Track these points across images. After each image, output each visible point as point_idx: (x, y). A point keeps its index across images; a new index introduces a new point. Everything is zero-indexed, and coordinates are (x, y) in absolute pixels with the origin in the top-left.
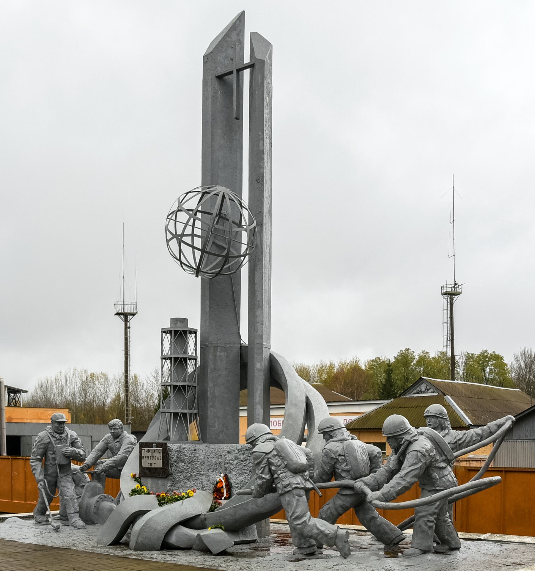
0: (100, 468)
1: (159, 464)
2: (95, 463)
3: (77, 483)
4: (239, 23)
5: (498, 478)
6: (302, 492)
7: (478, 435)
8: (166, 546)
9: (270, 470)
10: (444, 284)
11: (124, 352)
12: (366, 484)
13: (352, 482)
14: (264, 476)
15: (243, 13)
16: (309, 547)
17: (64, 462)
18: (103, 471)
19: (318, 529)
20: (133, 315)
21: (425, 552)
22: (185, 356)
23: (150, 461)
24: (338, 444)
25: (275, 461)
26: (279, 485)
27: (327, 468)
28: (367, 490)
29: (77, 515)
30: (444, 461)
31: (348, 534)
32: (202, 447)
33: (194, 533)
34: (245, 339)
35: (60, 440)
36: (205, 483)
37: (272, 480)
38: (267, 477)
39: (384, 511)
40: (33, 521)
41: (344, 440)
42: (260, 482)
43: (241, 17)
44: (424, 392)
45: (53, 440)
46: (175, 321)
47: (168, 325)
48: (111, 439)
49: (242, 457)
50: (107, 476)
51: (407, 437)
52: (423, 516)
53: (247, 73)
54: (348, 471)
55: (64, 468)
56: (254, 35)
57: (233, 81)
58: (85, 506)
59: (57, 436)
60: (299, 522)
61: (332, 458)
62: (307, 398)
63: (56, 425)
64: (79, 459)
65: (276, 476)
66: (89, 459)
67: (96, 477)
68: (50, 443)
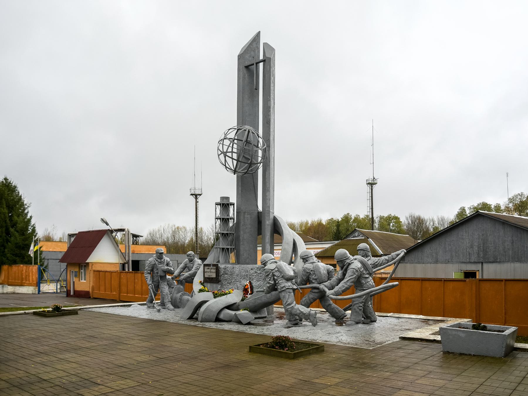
1: (214, 275)
2: (179, 275)
3: (170, 286)
5: (397, 283)
6: (291, 291)
7: (386, 260)
8: (218, 320)
9: (274, 279)
12: (326, 286)
15: (259, 32)
17: (163, 274)
18: (183, 279)
19: (300, 310)
20: (200, 195)
22: (228, 217)
23: (209, 274)
24: (311, 265)
25: (277, 274)
26: (279, 287)
27: (304, 278)
28: (326, 290)
30: (368, 274)
31: (316, 313)
33: (233, 313)
34: (260, 208)
36: (239, 286)
37: (275, 284)
38: (272, 282)
39: (335, 301)
40: (146, 306)
41: (314, 262)
42: (268, 285)
43: (258, 35)
45: (157, 262)
46: (222, 198)
47: (219, 201)
48: (188, 262)
49: (259, 272)
50: (186, 282)
51: (348, 261)
54: (316, 279)
55: (163, 278)
56: (265, 44)
57: (254, 69)
59: (159, 260)
62: (294, 240)
64: (171, 273)
65: (277, 282)
66: (176, 273)
67: (180, 282)
68: (155, 264)
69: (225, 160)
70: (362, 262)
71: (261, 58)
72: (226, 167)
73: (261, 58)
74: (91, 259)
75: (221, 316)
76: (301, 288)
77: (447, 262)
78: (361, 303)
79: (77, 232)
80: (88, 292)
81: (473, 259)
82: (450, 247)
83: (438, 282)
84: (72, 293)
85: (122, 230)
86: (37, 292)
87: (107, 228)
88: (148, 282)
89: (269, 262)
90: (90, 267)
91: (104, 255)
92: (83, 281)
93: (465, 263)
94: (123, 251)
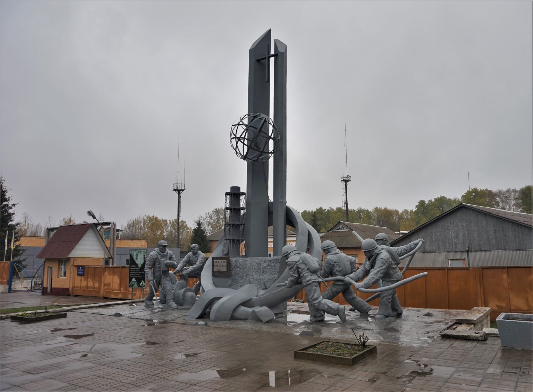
0: (185, 272)
1: (225, 269)
2: (182, 270)
4: (268, 34)
5: (426, 273)
6: (317, 284)
7: (405, 249)
8: (233, 318)
10: (342, 176)
11: (177, 210)
12: (351, 278)
13: (342, 278)
14: (294, 275)
15: (271, 30)
16: (320, 316)
17: (166, 269)
18: (187, 274)
19: (328, 306)
20: (183, 190)
21: (387, 317)
24: (333, 256)
26: (303, 280)
27: (327, 270)
28: (353, 282)
29: (172, 300)
30: (395, 264)
32: (248, 259)
33: (250, 310)
34: (271, 198)
35: (163, 256)
36: (251, 280)
37: (299, 277)
38: (297, 276)
39: (364, 295)
41: (337, 253)
42: (292, 278)
44: (341, 229)
45: (159, 256)
47: (229, 191)
50: (189, 277)
51: (376, 251)
52: (386, 296)
53: (272, 60)
54: (340, 271)
55: (166, 273)
57: (266, 62)
58: (176, 295)
59: (162, 254)
60: (317, 302)
61: (331, 264)
62: (308, 230)
63: (162, 247)
64: (174, 267)
65: (302, 275)
66: (179, 267)
67: (182, 277)
68: (157, 258)
69: (237, 146)
70: (389, 252)
71: (272, 52)
72: (236, 152)
73: (272, 52)
74: (72, 255)
75: (238, 314)
76: (326, 281)
77: (434, 251)
78: (389, 295)
79: (58, 226)
80: (68, 289)
81: (459, 248)
82: (436, 238)
83: (441, 271)
84: (49, 290)
85: (108, 224)
86: (7, 291)
87: (95, 221)
88: (149, 278)
89: (292, 253)
90: (71, 263)
91: (88, 250)
92: (63, 277)
93: (451, 252)
94: (108, 246)
